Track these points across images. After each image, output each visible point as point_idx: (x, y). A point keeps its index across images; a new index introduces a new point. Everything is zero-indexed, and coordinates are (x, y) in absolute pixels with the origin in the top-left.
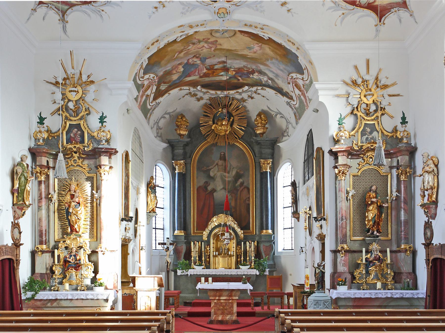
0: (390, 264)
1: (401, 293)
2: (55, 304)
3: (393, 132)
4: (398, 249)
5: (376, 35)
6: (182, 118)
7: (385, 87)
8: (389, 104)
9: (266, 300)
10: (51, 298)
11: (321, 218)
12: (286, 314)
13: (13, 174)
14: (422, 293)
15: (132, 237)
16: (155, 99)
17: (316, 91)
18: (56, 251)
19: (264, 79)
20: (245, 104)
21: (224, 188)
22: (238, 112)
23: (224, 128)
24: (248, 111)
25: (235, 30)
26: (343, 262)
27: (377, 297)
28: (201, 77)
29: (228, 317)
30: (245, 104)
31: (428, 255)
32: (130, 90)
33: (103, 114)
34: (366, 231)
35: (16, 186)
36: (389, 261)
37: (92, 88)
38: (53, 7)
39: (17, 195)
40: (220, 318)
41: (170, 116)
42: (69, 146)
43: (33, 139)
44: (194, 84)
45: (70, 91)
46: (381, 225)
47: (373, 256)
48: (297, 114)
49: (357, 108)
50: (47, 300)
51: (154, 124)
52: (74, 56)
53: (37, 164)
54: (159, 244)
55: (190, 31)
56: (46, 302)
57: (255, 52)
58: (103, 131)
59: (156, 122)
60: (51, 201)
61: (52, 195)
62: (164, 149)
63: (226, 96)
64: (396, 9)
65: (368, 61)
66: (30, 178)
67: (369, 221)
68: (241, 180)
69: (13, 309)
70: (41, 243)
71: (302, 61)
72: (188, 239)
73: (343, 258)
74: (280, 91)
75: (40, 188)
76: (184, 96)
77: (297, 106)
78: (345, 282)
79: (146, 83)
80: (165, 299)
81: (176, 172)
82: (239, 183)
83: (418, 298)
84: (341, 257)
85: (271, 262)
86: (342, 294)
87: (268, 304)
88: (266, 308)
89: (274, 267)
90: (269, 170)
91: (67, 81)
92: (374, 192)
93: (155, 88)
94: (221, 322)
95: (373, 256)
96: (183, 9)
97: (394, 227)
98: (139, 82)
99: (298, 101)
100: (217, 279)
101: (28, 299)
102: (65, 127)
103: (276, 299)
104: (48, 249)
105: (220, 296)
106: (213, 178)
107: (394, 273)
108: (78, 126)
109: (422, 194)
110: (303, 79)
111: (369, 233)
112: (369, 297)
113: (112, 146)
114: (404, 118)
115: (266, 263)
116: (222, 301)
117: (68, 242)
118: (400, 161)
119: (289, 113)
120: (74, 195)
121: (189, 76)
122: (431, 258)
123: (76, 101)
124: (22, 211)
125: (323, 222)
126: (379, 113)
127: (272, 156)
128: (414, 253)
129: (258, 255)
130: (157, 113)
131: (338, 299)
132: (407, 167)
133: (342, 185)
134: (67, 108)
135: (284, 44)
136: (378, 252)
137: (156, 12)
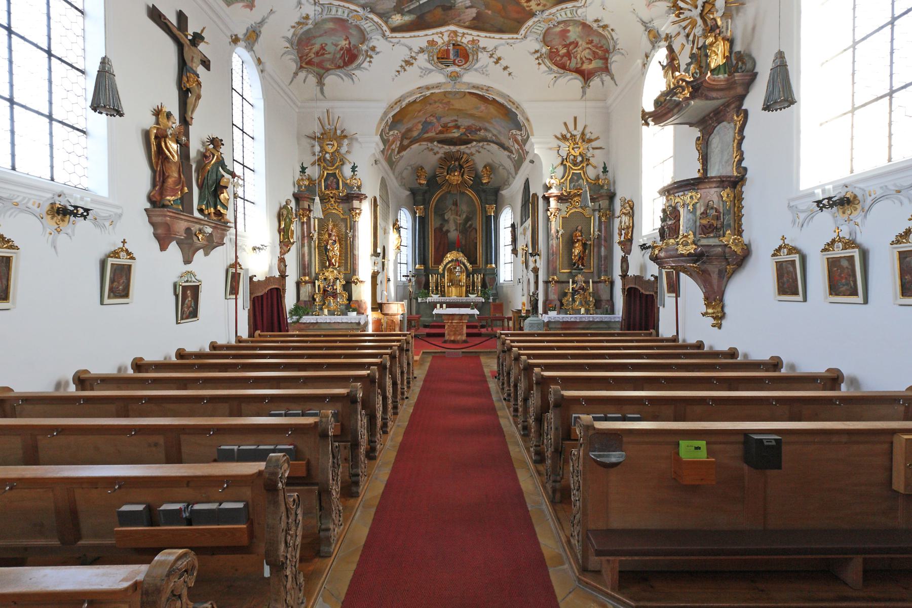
0: (592, 293)
1: (601, 317)
2: (316, 327)
3: (595, 180)
4: (599, 280)
5: (583, 96)
7: (590, 141)
8: (593, 156)
9: (490, 323)
10: (312, 321)
11: (535, 253)
12: (507, 335)
13: (280, 216)
14: (618, 318)
15: (380, 270)
16: (399, 153)
17: (532, 144)
18: (316, 281)
19: (489, 135)
20: (473, 157)
21: (456, 229)
22: (467, 165)
25: (465, 92)
28: (437, 134)
29: (459, 338)
30: (473, 157)
31: (624, 285)
32: (377, 144)
34: (572, 265)
35: (283, 226)
36: (591, 290)
37: (346, 142)
38: (312, 71)
40: (452, 338)
41: (412, 168)
43: (296, 186)
44: (431, 140)
45: (328, 144)
47: (578, 286)
48: (516, 166)
49: (566, 159)
50: (309, 323)
52: (330, 114)
53: (300, 207)
54: (403, 276)
55: (427, 93)
56: (309, 325)
57: (481, 112)
58: (355, 179)
62: (407, 196)
63: (458, 151)
64: (600, 73)
65: (575, 119)
66: (294, 219)
67: (575, 256)
68: (470, 223)
69: (280, 331)
70: (304, 275)
71: (520, 118)
72: (427, 272)
73: (553, 288)
74: (502, 146)
77: (516, 158)
78: (555, 308)
79: (391, 138)
80: (408, 322)
81: (417, 215)
82: (468, 225)
83: (615, 322)
84: (552, 286)
85: (494, 292)
87: (491, 326)
88: (490, 329)
89: (496, 296)
90: (493, 214)
91: (325, 136)
92: (579, 231)
93: (398, 143)
94: (453, 342)
95: (578, 286)
96: (421, 72)
97: (596, 261)
98: (385, 138)
100: (450, 305)
101: (293, 322)
103: (498, 322)
105: (453, 320)
106: (447, 221)
107: (596, 300)
108: (334, 175)
110: (521, 135)
113: (363, 192)
114: (605, 168)
115: (490, 292)
116: (454, 324)
117: (327, 274)
119: (509, 164)
121: (427, 132)
122: (627, 288)
123: (332, 153)
125: (537, 257)
127: (496, 202)
128: (612, 283)
129: (484, 285)
130: (402, 164)
131: (549, 322)
132: (607, 210)
134: (325, 159)
135: (506, 104)
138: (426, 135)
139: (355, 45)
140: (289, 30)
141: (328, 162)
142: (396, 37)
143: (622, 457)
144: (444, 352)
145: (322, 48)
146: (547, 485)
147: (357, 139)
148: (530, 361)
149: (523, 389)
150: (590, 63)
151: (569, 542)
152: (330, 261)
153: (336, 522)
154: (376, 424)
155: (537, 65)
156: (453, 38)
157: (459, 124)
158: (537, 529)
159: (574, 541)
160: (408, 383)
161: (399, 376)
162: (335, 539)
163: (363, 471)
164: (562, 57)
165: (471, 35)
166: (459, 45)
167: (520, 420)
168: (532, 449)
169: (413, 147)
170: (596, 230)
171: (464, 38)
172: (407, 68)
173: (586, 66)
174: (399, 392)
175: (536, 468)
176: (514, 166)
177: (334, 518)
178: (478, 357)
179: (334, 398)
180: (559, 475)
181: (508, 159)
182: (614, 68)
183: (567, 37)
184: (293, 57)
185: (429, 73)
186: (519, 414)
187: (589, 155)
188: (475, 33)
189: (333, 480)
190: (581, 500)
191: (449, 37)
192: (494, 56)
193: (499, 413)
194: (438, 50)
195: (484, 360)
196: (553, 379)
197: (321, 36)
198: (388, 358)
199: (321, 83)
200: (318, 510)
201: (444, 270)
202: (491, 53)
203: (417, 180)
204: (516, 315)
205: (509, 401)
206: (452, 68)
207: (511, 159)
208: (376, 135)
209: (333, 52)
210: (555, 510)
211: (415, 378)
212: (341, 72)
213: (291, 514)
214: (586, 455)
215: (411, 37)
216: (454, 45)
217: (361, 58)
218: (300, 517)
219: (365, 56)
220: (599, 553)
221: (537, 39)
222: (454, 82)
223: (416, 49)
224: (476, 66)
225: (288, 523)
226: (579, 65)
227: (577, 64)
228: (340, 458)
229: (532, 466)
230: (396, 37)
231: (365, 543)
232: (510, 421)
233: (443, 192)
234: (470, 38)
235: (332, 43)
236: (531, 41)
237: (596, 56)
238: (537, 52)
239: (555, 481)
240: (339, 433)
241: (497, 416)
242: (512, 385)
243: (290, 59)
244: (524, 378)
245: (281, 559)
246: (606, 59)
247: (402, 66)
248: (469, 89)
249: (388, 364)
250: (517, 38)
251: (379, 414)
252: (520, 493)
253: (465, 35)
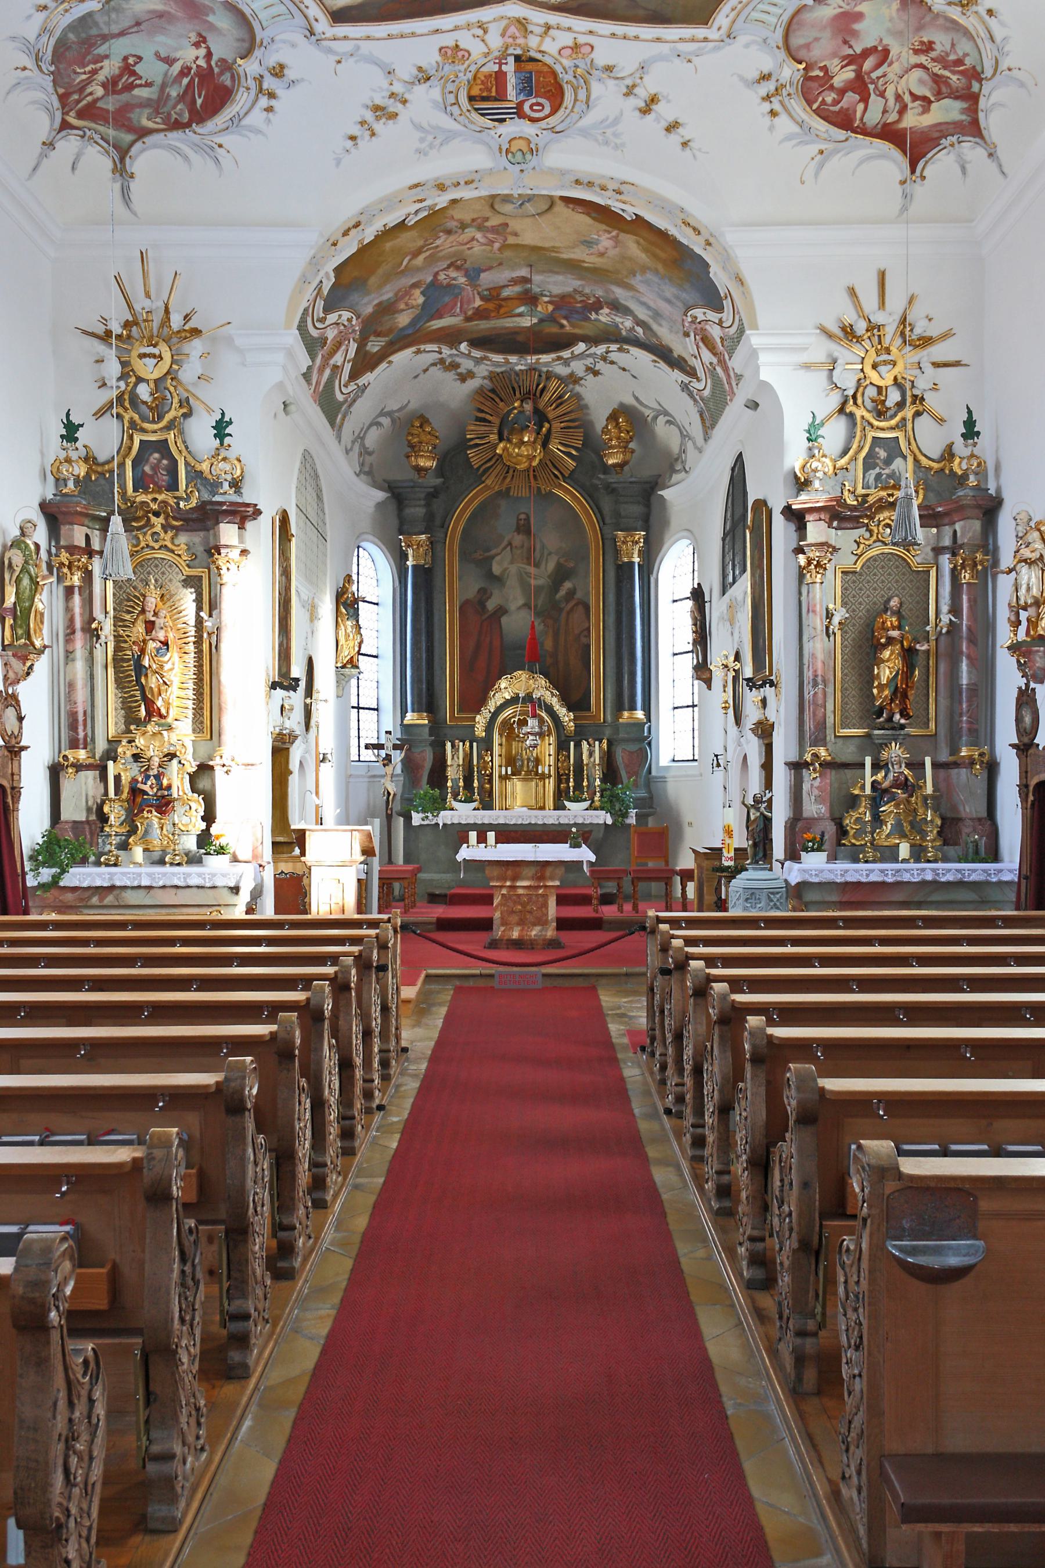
2: (109, 899)
3: (942, 458)
4: (951, 759)
6: (421, 426)
7: (926, 341)
8: (935, 387)
9: (628, 888)
10: (98, 883)
11: (763, 679)
12: (675, 923)
14: (1010, 871)
15: (299, 729)
16: (354, 376)
17: (754, 354)
18: (110, 764)
20: (578, 388)
21: (527, 605)
23: (528, 450)
24: (586, 407)
25: (551, 197)
26: (816, 792)
27: (899, 879)
28: (468, 319)
29: (534, 932)
30: (578, 388)
31: (1024, 773)
32: (290, 353)
33: (223, 414)
34: (872, 714)
36: (929, 789)
37: (195, 347)
38: (97, 137)
39: (12, 622)
40: (515, 934)
41: (393, 421)
42: (142, 498)
43: (51, 480)
44: (450, 337)
45: (142, 356)
46: (911, 698)
47: (891, 776)
48: (706, 415)
49: (854, 397)
50: (89, 888)
51: (353, 442)
52: (151, 265)
53: (62, 543)
54: (367, 747)
56: (87, 894)
57: (602, 255)
58: (224, 459)
59: (358, 437)
60: (98, 637)
61: (99, 623)
62: (379, 506)
63: (532, 369)
64: (954, 139)
65: (882, 276)
66: (44, 578)
67: (881, 687)
68: (568, 585)
70: (74, 744)
71: (718, 275)
72: (438, 734)
73: (817, 783)
74: (664, 354)
75: (70, 605)
76: (427, 370)
77: (706, 393)
78: (821, 843)
79: (331, 334)
81: (409, 563)
82: (562, 592)
83: (1000, 883)
84: (811, 780)
85: (642, 793)
86: (814, 873)
87: (633, 898)
88: (628, 907)
92: (893, 613)
93: (353, 347)
94: (517, 944)
95: (891, 776)
96: (422, 140)
97: (943, 702)
98: (315, 333)
99: (709, 381)
100: (508, 834)
101: (42, 886)
102: (130, 448)
103: (653, 884)
104: (91, 761)
105: (515, 878)
106: (499, 580)
107: (943, 819)
108: (162, 447)
109: (1013, 618)
110: (720, 323)
111: (882, 719)
112: (880, 879)
116: (520, 891)
117: (140, 742)
118: (959, 534)
119: (686, 411)
120: (153, 623)
123: (156, 381)
124: (24, 664)
125: (768, 691)
126: (908, 412)
128: (992, 768)
129: (610, 775)
130: (362, 411)
131: (803, 886)
133: (814, 597)
134: (135, 400)
135: (673, 231)
136: (903, 765)
137: (353, 150)
138: (437, 324)
139: (223, 61)
140: (29, 17)
141: (143, 408)
142: (345, 38)
143: (974, 1255)
144: (491, 976)
145: (128, 69)
146: (781, 1346)
147: (229, 340)
148: (739, 998)
149: (718, 1077)
150: (926, 110)
151: (836, 1495)
152: (149, 704)
153: (191, 1439)
154: (293, 1176)
155: (768, 118)
156: (514, 38)
157: (536, 289)
158: (749, 1466)
159: (848, 1492)
160: (385, 1064)
161: (357, 1041)
162: (187, 1485)
163: (260, 1306)
164: (842, 92)
165: (569, 29)
166: (532, 60)
167: (710, 1169)
168: (742, 1250)
169: (397, 358)
170: (945, 608)
171: (548, 40)
172: (378, 127)
173: (914, 120)
174: (358, 1091)
175: (753, 1301)
176: (701, 416)
177: (185, 1427)
178: (593, 989)
179: (179, 1097)
180: (813, 1316)
181: (685, 395)
182: (992, 122)
183: (855, 34)
184: (41, 96)
185: (446, 141)
186: (707, 1152)
187: (922, 384)
188: (581, 24)
189: (182, 1320)
190: (864, 1374)
191: (503, 35)
192: (636, 91)
193: (652, 1152)
194: (470, 76)
195: (607, 999)
196: (802, 1048)
197: (122, 34)
198: (327, 990)
199: (121, 170)
200: (141, 1403)
201: (489, 728)
202: (629, 82)
203: (408, 457)
204: (706, 864)
205: (680, 1115)
206: (515, 127)
207: (691, 395)
208: (288, 327)
209: (159, 80)
210: (802, 1416)
211: (405, 1050)
212: (178, 140)
213: (79, 1396)
214: (878, 1249)
215: (390, 37)
216: (518, 58)
217: (242, 100)
218: (100, 1410)
219: (253, 92)
220: (911, 1514)
221: (765, 41)
222: (518, 167)
223: (406, 72)
224: (588, 120)
225: (70, 1420)
226: (892, 117)
227: (885, 111)
228: (201, 1262)
229: (739, 1296)
230: (345, 38)
231: (268, 1499)
232: (681, 1175)
233: (488, 493)
234: (566, 39)
235: (157, 55)
236: (747, 46)
237: (944, 89)
238: (765, 77)
239: (801, 1333)
240: (193, 1197)
241: (644, 1160)
242: (688, 1068)
243: (34, 102)
244: (722, 1050)
245: (57, 1514)
246: (973, 99)
247: (363, 123)
248: (563, 187)
249: (328, 1006)
250: (706, 40)
251: (304, 1148)
252: (704, 1368)
253: (552, 32)
